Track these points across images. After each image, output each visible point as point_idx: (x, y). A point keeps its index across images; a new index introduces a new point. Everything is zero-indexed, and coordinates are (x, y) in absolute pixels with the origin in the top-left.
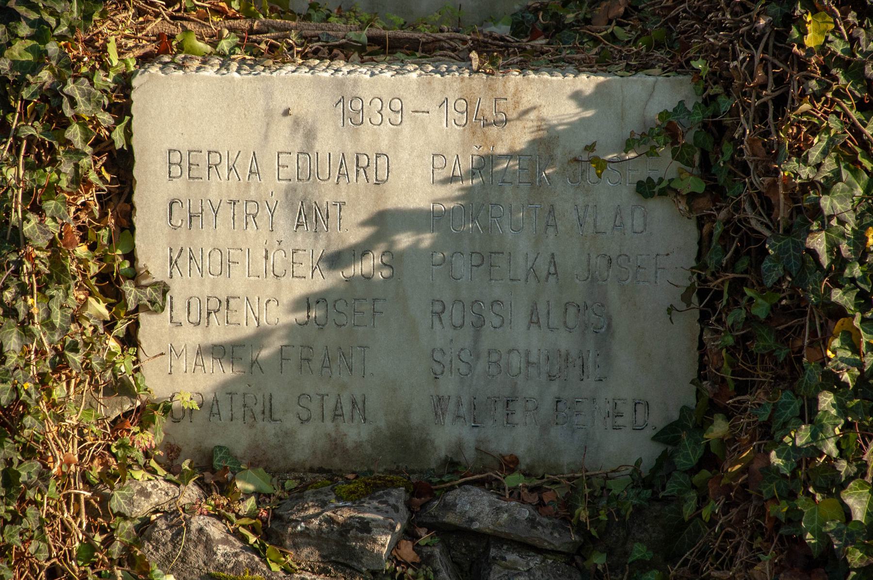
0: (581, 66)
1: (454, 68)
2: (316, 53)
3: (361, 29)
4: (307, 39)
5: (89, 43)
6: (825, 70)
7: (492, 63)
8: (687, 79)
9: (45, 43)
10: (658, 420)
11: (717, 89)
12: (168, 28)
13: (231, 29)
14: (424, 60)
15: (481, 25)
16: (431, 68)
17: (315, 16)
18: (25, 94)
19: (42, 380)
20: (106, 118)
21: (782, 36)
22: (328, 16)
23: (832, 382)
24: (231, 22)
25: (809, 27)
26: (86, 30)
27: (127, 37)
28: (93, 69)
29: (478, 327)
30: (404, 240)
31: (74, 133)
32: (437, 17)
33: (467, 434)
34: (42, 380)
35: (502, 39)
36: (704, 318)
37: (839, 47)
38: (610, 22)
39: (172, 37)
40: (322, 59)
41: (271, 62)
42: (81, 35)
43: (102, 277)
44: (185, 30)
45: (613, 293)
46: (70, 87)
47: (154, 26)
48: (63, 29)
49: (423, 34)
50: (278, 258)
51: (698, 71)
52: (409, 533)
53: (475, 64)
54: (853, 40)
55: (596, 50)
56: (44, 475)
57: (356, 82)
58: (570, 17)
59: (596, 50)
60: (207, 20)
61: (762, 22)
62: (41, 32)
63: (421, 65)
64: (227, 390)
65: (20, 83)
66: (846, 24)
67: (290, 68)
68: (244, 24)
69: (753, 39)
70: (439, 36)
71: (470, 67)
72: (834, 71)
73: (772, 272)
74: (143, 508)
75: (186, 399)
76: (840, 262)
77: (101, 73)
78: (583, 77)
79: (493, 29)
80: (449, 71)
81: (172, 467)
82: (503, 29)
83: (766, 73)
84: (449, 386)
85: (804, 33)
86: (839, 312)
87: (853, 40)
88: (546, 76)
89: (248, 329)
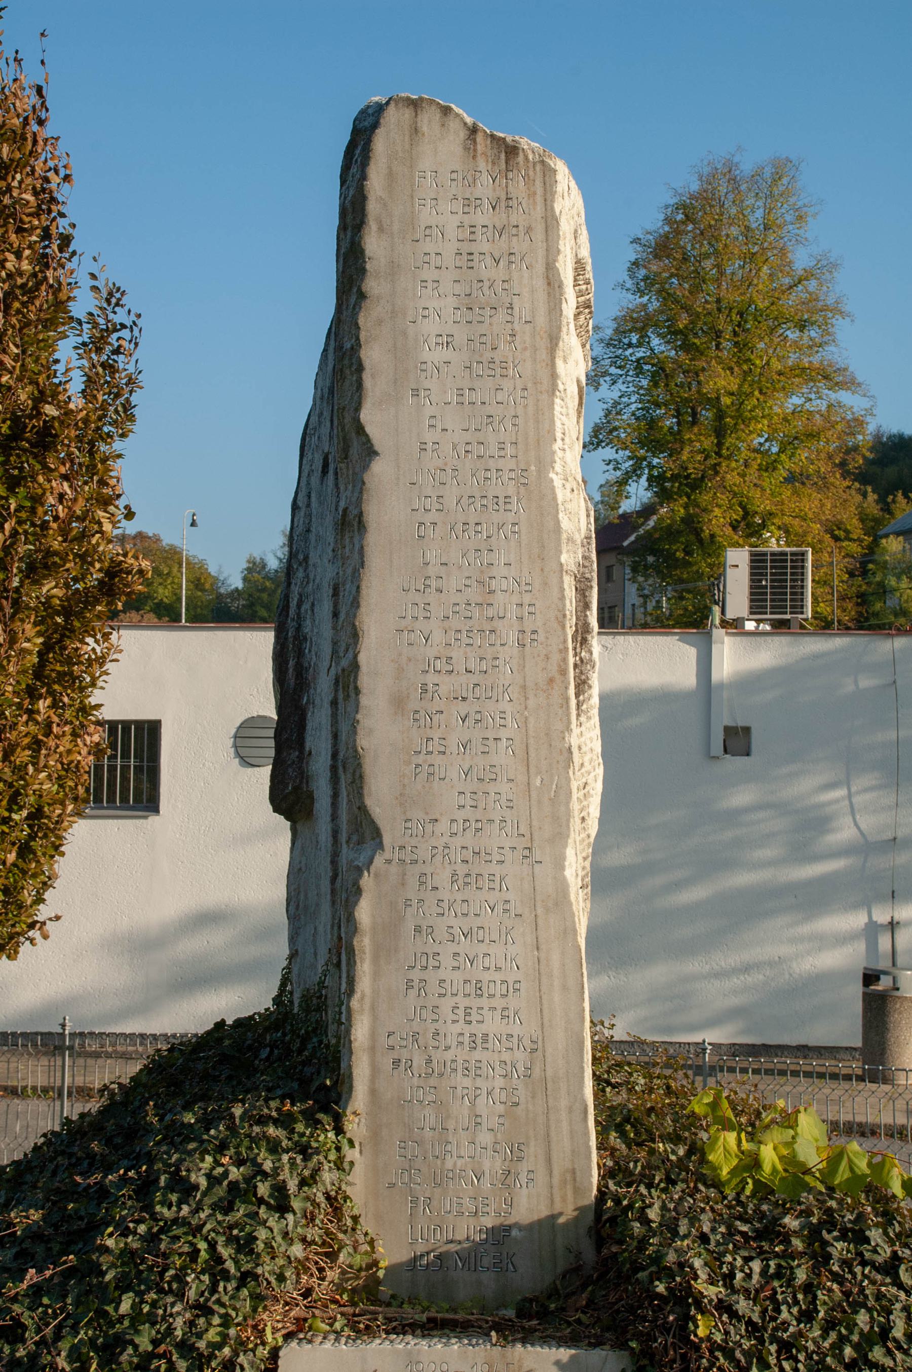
0: (562, 1342)
1: (481, 1341)
2: (394, 1331)
3: (423, 1312)
4: (389, 1320)
5: (255, 1327)
6: (711, 1352)
7: (505, 1339)
8: (626, 1353)
9: (228, 1328)
11: (645, 1362)
12: (303, 1315)
13: (342, 1314)
14: (462, 1335)
15: (497, 1309)
16: (466, 1342)
17: (394, 1303)
18: (213, 1364)
21: (685, 1327)
22: (402, 1303)
24: (342, 1309)
25: (700, 1323)
26: (254, 1318)
27: (278, 1321)
28: (256, 1345)
32: (470, 1304)
35: (510, 1320)
37: (718, 1338)
38: (577, 1311)
39: (305, 1320)
40: (397, 1334)
41: (366, 1337)
42: (250, 1322)
44: (314, 1316)
46: (242, 1359)
47: (295, 1312)
48: (240, 1319)
49: (460, 1316)
51: (633, 1349)
53: (494, 1340)
54: (727, 1333)
55: (569, 1330)
57: (419, 1351)
58: (553, 1306)
59: (569, 1330)
60: (327, 1307)
61: (671, 1318)
62: (226, 1322)
63: (459, 1338)
65: (212, 1356)
66: (722, 1322)
67: (378, 1341)
68: (349, 1310)
69: (666, 1329)
70: (471, 1317)
71: (490, 1341)
72: (717, 1354)
77: (261, 1347)
78: (562, 1350)
79: (504, 1312)
80: (478, 1344)
82: (510, 1313)
83: (675, 1352)
85: (697, 1327)
87: (727, 1333)
88: (539, 1349)
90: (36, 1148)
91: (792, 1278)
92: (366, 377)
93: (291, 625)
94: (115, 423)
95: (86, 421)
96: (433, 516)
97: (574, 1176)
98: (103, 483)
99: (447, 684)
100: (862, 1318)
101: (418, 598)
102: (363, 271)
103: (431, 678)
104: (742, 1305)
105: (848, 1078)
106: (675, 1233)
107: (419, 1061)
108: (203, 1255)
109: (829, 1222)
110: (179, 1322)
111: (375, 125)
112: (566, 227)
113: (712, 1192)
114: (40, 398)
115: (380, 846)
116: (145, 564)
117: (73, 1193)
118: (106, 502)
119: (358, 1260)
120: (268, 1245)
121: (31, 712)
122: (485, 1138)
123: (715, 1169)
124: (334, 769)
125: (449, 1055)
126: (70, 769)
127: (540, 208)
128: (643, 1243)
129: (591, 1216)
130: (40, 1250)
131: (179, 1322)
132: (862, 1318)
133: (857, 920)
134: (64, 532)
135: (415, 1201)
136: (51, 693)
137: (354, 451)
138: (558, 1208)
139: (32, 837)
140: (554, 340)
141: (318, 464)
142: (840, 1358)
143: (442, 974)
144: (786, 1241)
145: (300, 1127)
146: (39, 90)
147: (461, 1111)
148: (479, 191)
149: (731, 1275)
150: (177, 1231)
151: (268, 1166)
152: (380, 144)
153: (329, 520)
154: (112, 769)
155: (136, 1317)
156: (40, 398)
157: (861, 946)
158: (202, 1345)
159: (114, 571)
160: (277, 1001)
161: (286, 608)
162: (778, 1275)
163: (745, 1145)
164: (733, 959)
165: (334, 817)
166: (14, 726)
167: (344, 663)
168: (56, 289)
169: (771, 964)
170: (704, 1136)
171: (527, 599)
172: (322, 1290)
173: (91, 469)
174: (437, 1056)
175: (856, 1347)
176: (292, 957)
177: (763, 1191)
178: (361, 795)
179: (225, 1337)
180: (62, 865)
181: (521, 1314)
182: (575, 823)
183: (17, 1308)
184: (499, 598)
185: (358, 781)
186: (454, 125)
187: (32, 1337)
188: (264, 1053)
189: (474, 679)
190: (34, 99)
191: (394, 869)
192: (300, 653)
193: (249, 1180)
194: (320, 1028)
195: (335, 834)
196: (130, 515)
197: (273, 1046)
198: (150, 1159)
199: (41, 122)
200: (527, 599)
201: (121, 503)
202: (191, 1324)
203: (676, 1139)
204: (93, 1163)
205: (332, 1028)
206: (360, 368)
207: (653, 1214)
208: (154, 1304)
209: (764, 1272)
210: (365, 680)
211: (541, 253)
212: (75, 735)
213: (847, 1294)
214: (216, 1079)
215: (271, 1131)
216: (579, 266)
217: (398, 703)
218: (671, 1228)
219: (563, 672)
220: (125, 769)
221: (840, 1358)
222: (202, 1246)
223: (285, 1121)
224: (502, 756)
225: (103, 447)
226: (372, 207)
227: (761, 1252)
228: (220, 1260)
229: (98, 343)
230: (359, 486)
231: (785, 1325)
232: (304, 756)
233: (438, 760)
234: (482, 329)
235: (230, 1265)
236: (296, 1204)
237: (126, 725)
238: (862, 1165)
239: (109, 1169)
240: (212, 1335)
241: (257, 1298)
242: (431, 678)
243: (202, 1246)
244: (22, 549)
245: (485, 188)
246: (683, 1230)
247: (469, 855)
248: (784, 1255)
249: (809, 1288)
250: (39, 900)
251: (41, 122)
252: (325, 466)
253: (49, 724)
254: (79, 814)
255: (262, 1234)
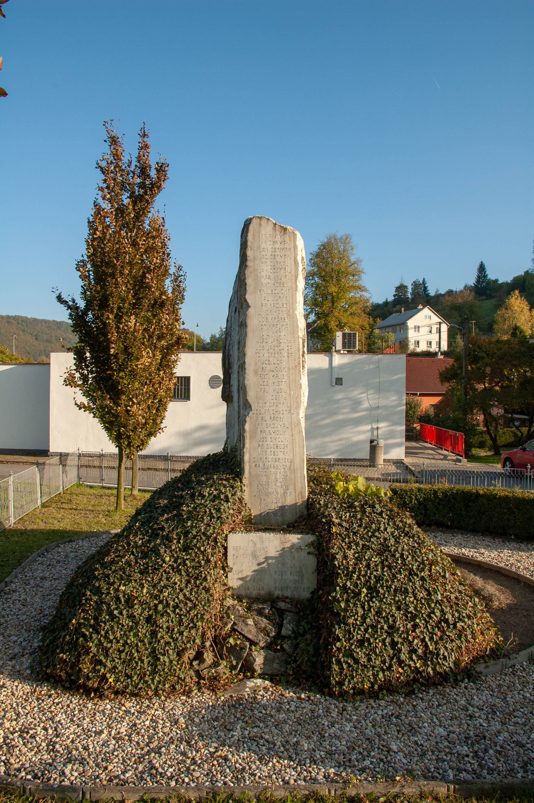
0: (299, 533)
10: (311, 590)
19: (213, 584)
20: (224, 541)
23: (338, 585)
29: (282, 575)
30: (270, 561)
31: (219, 544)
33: (280, 593)
34: (213, 584)
36: (318, 574)
37: (338, 532)
43: (223, 567)
45: (304, 570)
50: (250, 564)
52: (271, 609)
56: (213, 599)
62: (214, 528)
64: (242, 585)
69: (325, 530)
73: (329, 567)
74: (228, 605)
75: (235, 587)
76: (339, 566)
81: (233, 598)
82: (285, 527)
84: (277, 585)
86: (339, 574)
89: (245, 575)
90: (165, 485)
91: (357, 517)
92: (247, 287)
93: (227, 352)
94: (179, 300)
95: (172, 300)
96: (265, 323)
97: (301, 494)
98: (177, 315)
99: (269, 367)
100: (373, 526)
101: (261, 345)
102: (246, 260)
103: (264, 366)
104: (344, 524)
105: (367, 466)
106: (327, 507)
107: (261, 465)
108: (208, 512)
109: (366, 503)
110: (203, 528)
111: (250, 223)
112: (299, 248)
113: (337, 497)
114: (162, 294)
115: (251, 410)
116: (187, 336)
117: (175, 496)
118: (177, 320)
119: (246, 514)
120: (224, 510)
121: (158, 375)
122: (279, 484)
123: (337, 491)
124: (238, 389)
125: (269, 464)
126: (169, 389)
127: (292, 244)
128: (319, 510)
129: (306, 503)
130: (167, 509)
131: (203, 528)
132: (373, 526)
133: (369, 427)
134: (167, 328)
135: (261, 500)
136: (163, 370)
137: (244, 306)
138: (297, 501)
139: (159, 406)
140: (296, 277)
141: (234, 310)
142: (368, 535)
143: (267, 443)
144: (355, 508)
145: (231, 481)
146: (163, 218)
147: (273, 477)
148: (277, 239)
149: (342, 517)
150: (201, 506)
151: (223, 491)
152: (251, 228)
153: (237, 324)
154: (178, 389)
155: (192, 527)
156: (162, 294)
157: (370, 434)
158: (208, 533)
159: (179, 338)
160: (224, 449)
161: (225, 347)
162: (353, 516)
163: (345, 485)
164: (337, 437)
165: (239, 402)
166: (154, 378)
167: (242, 362)
168: (166, 267)
169: (347, 438)
170: (334, 483)
171: (290, 345)
172: (237, 521)
173: (174, 312)
174: (266, 464)
175: (372, 532)
176: (228, 438)
177: (349, 496)
178: (246, 397)
179: (214, 532)
180: (167, 414)
181: (288, 527)
182: (302, 404)
183: (163, 523)
184: (282, 344)
185: (245, 393)
186: (270, 223)
187: (166, 530)
188: (221, 463)
189: (276, 366)
190: (162, 221)
191: (255, 416)
192: (229, 359)
193: (219, 494)
194: (235, 456)
195: (239, 406)
196: (183, 324)
197: (223, 461)
198: (194, 489)
199: (163, 226)
200: (290, 345)
201: (181, 320)
202: (206, 528)
203: (327, 484)
204: (179, 489)
205: (239, 457)
206: (246, 285)
207: (322, 502)
208: (196, 524)
209: (350, 516)
210: (247, 366)
211: (293, 255)
212: (169, 380)
213: (370, 520)
214: (209, 469)
215: (224, 482)
216: (303, 258)
217: (256, 372)
218: (326, 506)
219: (299, 364)
220: (181, 389)
221: (368, 535)
222: (208, 510)
223: (227, 480)
224: (283, 386)
225: (177, 306)
226: (249, 243)
227: (349, 511)
228: (212, 514)
229: (176, 280)
230: (245, 315)
231: (355, 528)
232: (230, 386)
233: (266, 387)
234: (278, 274)
235: (215, 515)
236: (231, 500)
237: (182, 377)
238: (374, 489)
239: (183, 491)
240: (211, 531)
241: (222, 523)
242: (264, 366)
243: (208, 510)
244: (157, 332)
245: (278, 238)
246: (329, 506)
247: (274, 412)
248: (355, 512)
249: (361, 519)
250: (161, 422)
251: (163, 226)
252: (236, 310)
253: (163, 377)
254: (171, 401)
255: (222, 507)
